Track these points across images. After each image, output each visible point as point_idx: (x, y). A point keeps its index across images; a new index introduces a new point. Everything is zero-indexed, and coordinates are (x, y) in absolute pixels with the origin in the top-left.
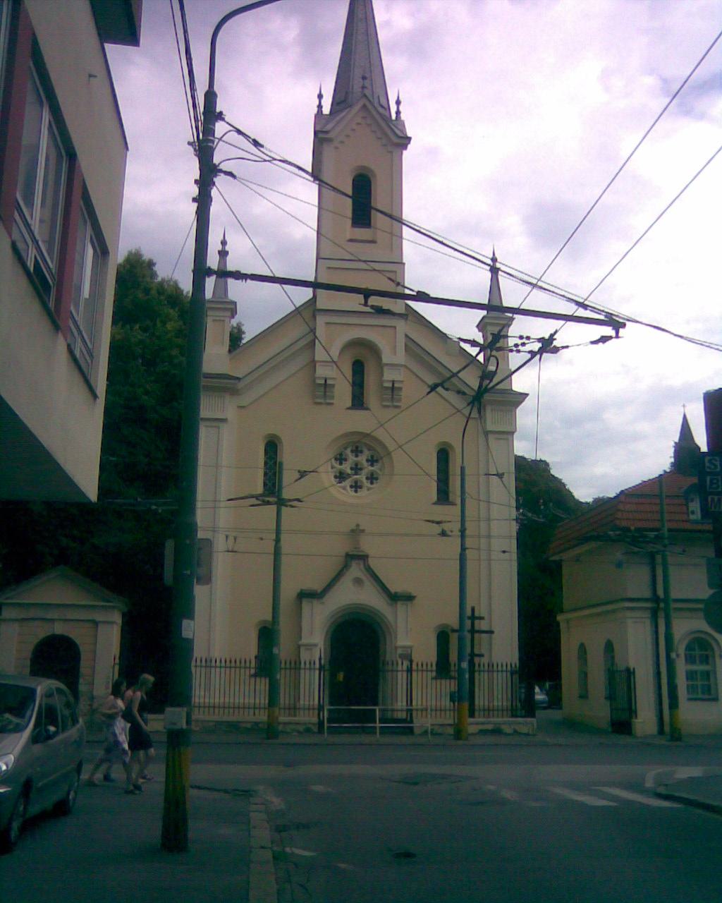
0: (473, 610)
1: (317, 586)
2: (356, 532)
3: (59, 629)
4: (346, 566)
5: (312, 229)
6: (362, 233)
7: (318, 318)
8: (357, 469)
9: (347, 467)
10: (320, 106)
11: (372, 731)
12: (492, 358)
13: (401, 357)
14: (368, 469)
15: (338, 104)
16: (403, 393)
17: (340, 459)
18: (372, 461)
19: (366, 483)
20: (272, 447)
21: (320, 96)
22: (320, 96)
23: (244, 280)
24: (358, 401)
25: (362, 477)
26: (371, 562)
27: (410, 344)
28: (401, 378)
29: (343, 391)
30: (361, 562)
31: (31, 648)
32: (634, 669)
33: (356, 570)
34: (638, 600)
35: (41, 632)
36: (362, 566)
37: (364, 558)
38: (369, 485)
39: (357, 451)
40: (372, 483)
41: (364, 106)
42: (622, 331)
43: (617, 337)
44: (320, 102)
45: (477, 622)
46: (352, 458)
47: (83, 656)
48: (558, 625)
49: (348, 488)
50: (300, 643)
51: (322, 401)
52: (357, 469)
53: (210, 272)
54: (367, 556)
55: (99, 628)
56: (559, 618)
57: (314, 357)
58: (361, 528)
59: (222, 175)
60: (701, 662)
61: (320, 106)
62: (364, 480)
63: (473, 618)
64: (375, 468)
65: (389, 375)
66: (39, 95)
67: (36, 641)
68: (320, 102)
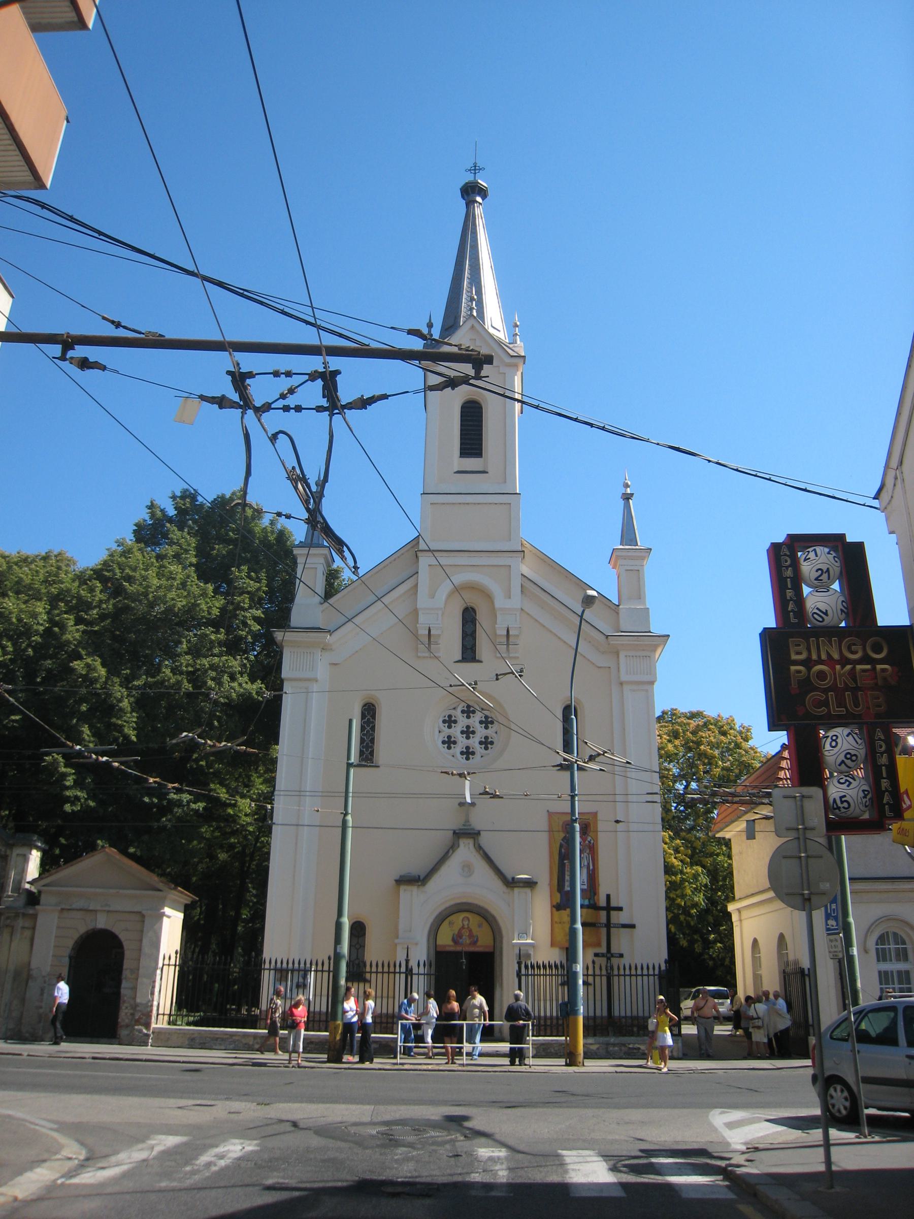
0: (608, 897)
3: (102, 922)
4: (453, 847)
6: (472, 463)
7: (420, 559)
8: (468, 732)
9: (462, 742)
12: (281, 436)
13: (516, 601)
14: (481, 732)
15: (446, 330)
17: (450, 721)
18: (487, 722)
19: (479, 749)
20: (369, 712)
24: (469, 653)
25: (474, 742)
26: (484, 840)
27: (528, 585)
31: (70, 943)
33: (465, 851)
34: (807, 871)
35: (80, 926)
36: (471, 845)
37: (473, 834)
38: (483, 751)
39: (468, 712)
40: (486, 748)
41: (473, 327)
42: (486, 370)
43: (478, 377)
45: (613, 913)
46: (462, 722)
47: (127, 954)
48: (729, 915)
49: (458, 755)
50: (396, 941)
52: (468, 732)
54: (478, 833)
55: (98, 916)
56: (731, 907)
57: (416, 605)
59: (121, 328)
60: (898, 959)
62: (477, 746)
63: (609, 908)
64: (490, 732)
66: (766, 644)
67: (76, 936)
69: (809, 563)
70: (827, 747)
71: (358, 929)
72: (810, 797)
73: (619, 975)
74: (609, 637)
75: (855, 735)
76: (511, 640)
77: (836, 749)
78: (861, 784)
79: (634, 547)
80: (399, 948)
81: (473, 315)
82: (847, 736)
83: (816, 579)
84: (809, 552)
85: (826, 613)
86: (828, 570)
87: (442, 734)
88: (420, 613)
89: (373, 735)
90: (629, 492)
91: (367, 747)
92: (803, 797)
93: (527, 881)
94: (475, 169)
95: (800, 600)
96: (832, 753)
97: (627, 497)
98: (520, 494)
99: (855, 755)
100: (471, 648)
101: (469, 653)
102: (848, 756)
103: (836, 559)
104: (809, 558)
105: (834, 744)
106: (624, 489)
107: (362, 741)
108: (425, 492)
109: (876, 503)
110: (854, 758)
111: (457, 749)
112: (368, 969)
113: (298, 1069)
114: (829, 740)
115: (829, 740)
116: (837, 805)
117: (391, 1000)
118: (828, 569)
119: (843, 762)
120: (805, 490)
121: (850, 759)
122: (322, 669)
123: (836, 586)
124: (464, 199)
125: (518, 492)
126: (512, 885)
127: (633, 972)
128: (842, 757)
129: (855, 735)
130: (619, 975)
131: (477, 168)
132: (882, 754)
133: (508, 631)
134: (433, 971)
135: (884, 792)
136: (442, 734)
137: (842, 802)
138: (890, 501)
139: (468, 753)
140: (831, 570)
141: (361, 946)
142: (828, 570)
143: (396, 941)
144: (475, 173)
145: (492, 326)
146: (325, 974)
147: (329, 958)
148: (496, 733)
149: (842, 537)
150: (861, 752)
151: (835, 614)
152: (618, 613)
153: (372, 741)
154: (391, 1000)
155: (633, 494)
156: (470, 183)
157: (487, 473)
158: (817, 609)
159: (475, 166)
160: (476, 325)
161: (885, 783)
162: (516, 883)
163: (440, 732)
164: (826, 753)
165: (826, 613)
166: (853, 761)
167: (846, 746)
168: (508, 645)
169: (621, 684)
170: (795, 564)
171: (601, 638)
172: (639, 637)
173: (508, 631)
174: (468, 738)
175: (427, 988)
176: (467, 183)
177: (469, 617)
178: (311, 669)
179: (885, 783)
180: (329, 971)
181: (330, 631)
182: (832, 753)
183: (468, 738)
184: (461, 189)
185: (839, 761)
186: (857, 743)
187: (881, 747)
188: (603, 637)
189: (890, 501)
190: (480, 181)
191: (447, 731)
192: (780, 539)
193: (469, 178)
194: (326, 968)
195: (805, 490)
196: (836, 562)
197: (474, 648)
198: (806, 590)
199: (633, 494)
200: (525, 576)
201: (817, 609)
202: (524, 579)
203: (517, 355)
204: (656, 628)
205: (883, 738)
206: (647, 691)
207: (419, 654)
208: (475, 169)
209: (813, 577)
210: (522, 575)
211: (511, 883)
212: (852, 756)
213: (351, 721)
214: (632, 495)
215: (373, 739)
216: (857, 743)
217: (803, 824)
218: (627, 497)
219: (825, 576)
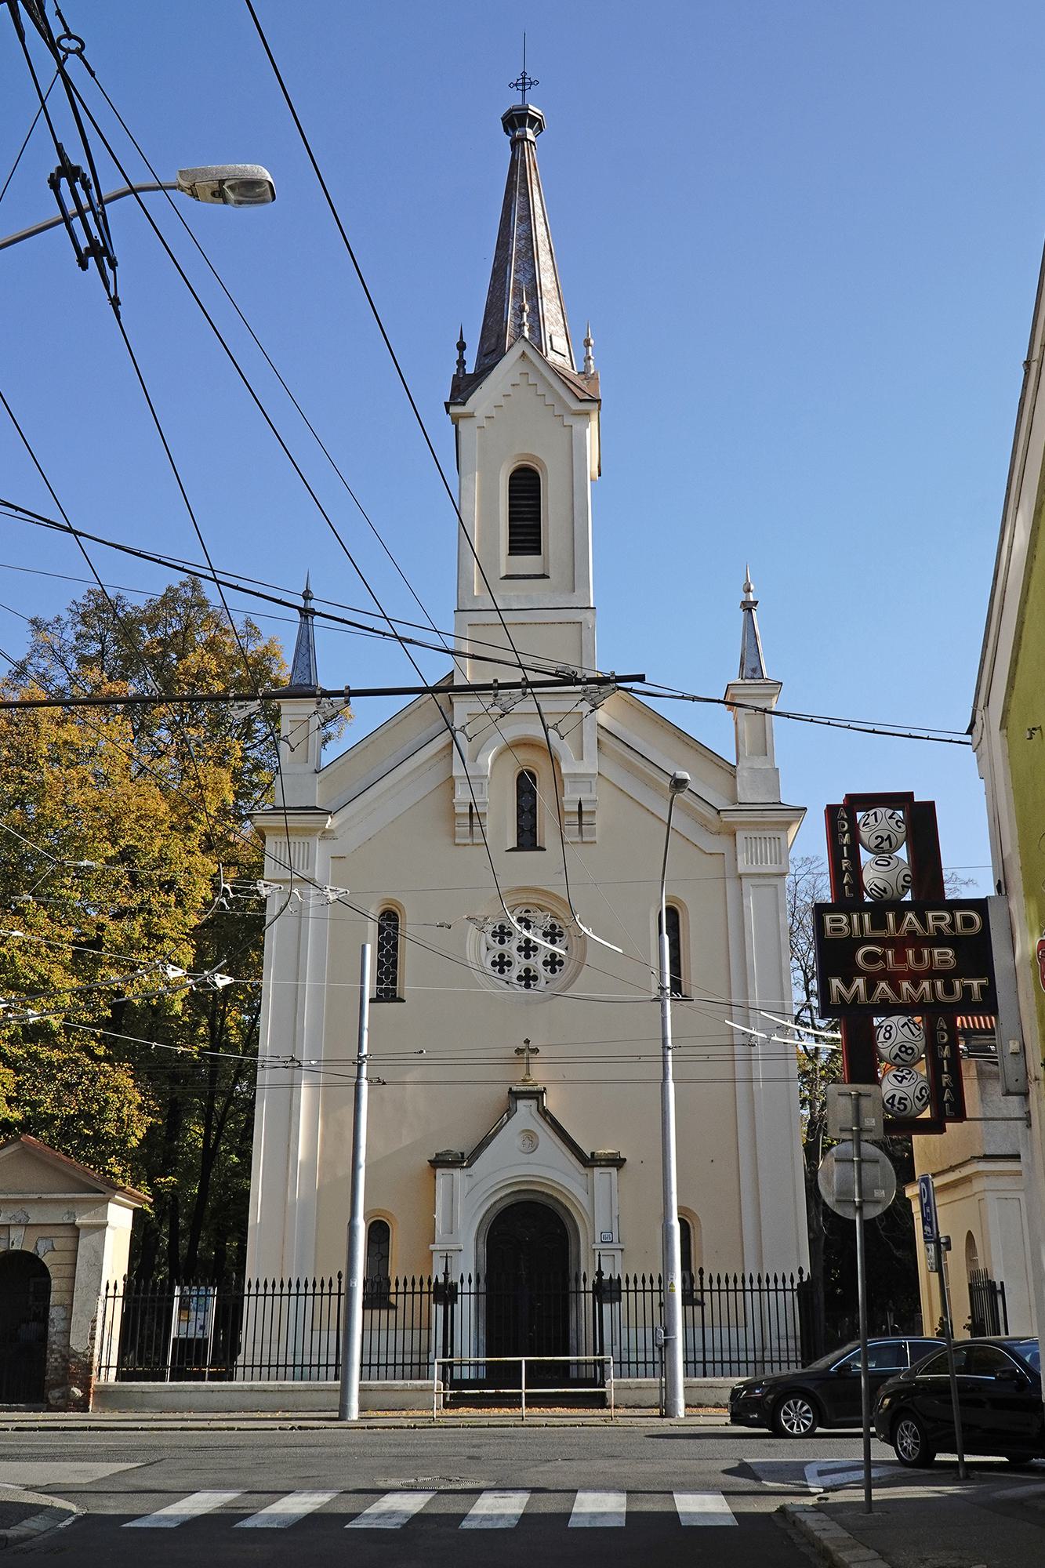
1: (458, 1144)
2: (526, 1052)
4: (510, 1111)
5: (510, 624)
6: (527, 563)
9: (519, 963)
10: (461, 363)
11: (513, 1402)
16: (598, 820)
19: (543, 973)
21: (461, 346)
22: (461, 346)
23: (970, 1322)
24: (527, 839)
25: (537, 962)
27: (605, 738)
28: (592, 796)
29: (503, 824)
30: (533, 1103)
32: (1002, 1283)
38: (550, 975)
40: (553, 971)
44: (461, 356)
51: (468, 841)
53: (669, 1048)
58: (532, 1045)
61: (461, 363)
65: (571, 797)
68: (461, 356)
69: (868, 829)
70: (881, 1038)
71: (379, 1233)
72: (869, 1096)
73: (628, 1291)
74: (721, 813)
75: (912, 1026)
76: (585, 819)
77: (890, 1042)
78: (918, 1081)
79: (758, 682)
80: (436, 1256)
81: (523, 337)
82: (903, 1026)
83: (876, 847)
84: (868, 815)
85: (885, 891)
86: (889, 837)
87: (492, 953)
88: (457, 782)
89: (395, 956)
90: (752, 600)
91: (387, 973)
92: (860, 1095)
93: (611, 1157)
94: (524, 83)
95: (857, 871)
96: (886, 1045)
97: (748, 607)
98: (595, 608)
99: (910, 1048)
100: (530, 831)
101: (527, 839)
102: (903, 1049)
103: (899, 824)
104: (868, 824)
105: (887, 1035)
106: (745, 595)
107: (380, 964)
108: (460, 609)
109: (968, 738)
110: (910, 1051)
111: (515, 972)
112: (393, 1289)
113: (299, 1431)
114: (883, 1030)
115: (883, 1030)
116: (893, 1101)
117: (741, 1330)
118: (889, 835)
119: (897, 1055)
120: (873, 731)
121: (906, 1052)
122: (319, 860)
123: (902, 853)
124: (507, 133)
125: (592, 606)
126: (590, 1164)
127: (723, 1286)
128: (896, 1050)
129: (912, 1026)
130: (628, 1291)
131: (527, 81)
132: (944, 1046)
133: (580, 806)
134: (483, 1288)
135: (945, 1088)
136: (492, 953)
137: (899, 1103)
138: (980, 742)
139: (528, 978)
140: (892, 836)
141: (383, 1257)
142: (889, 837)
143: (432, 1247)
144: (524, 78)
145: (552, 349)
146: (335, 1298)
147: (340, 1276)
148: (547, 983)
149: (910, 795)
150: (920, 1043)
151: (895, 891)
152: (735, 777)
153: (395, 964)
154: (741, 1330)
155: (757, 602)
156: (516, 110)
157: (548, 577)
158: (875, 885)
159: (524, 78)
160: (530, 353)
161: (945, 1079)
162: (597, 1160)
163: (488, 949)
164: (880, 1045)
165: (885, 891)
166: (908, 1054)
167: (900, 1038)
168: (580, 824)
169: (740, 877)
170: (854, 829)
171: (710, 814)
172: (764, 812)
173: (580, 806)
174: (527, 956)
175: (580, 1298)
176: (511, 111)
177: (526, 785)
178: (305, 867)
179: (945, 1079)
180: (339, 1294)
181: (331, 812)
182: (886, 1045)
183: (527, 956)
184: (503, 119)
185: (893, 1055)
186: (914, 1035)
187: (943, 1038)
188: (715, 812)
189: (980, 742)
190: (531, 107)
191: (498, 948)
192: (839, 800)
193: (514, 100)
194: (335, 1290)
195: (873, 731)
196: (900, 827)
197: (534, 830)
198: (865, 857)
199: (757, 602)
200: (602, 727)
201: (875, 885)
202: (601, 730)
203: (588, 398)
204: (789, 798)
205: (945, 1027)
206: (776, 886)
207: (457, 841)
208: (524, 83)
209: (873, 846)
210: (598, 725)
211: (589, 1161)
212: (907, 1049)
213: (364, 947)
214: (756, 603)
215: (396, 944)
216: (914, 1035)
217: (858, 1125)
218: (748, 607)
219: (886, 845)
